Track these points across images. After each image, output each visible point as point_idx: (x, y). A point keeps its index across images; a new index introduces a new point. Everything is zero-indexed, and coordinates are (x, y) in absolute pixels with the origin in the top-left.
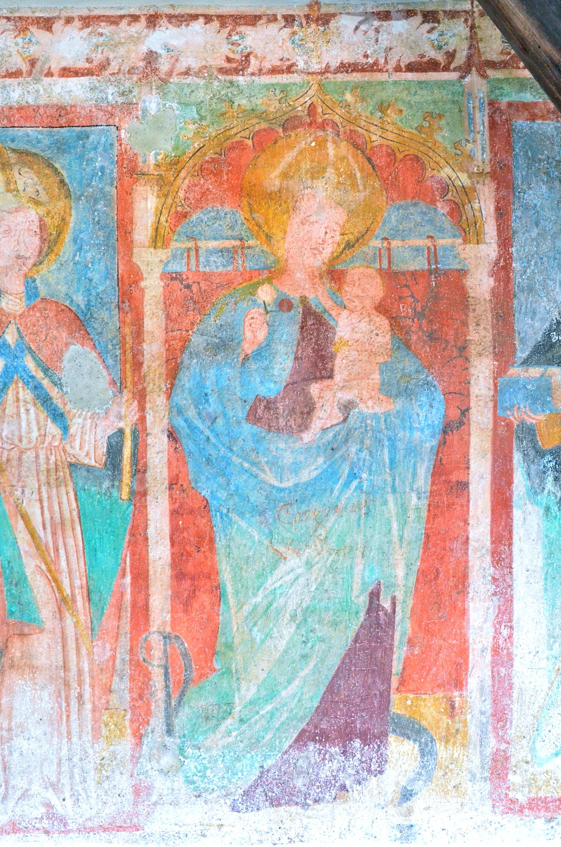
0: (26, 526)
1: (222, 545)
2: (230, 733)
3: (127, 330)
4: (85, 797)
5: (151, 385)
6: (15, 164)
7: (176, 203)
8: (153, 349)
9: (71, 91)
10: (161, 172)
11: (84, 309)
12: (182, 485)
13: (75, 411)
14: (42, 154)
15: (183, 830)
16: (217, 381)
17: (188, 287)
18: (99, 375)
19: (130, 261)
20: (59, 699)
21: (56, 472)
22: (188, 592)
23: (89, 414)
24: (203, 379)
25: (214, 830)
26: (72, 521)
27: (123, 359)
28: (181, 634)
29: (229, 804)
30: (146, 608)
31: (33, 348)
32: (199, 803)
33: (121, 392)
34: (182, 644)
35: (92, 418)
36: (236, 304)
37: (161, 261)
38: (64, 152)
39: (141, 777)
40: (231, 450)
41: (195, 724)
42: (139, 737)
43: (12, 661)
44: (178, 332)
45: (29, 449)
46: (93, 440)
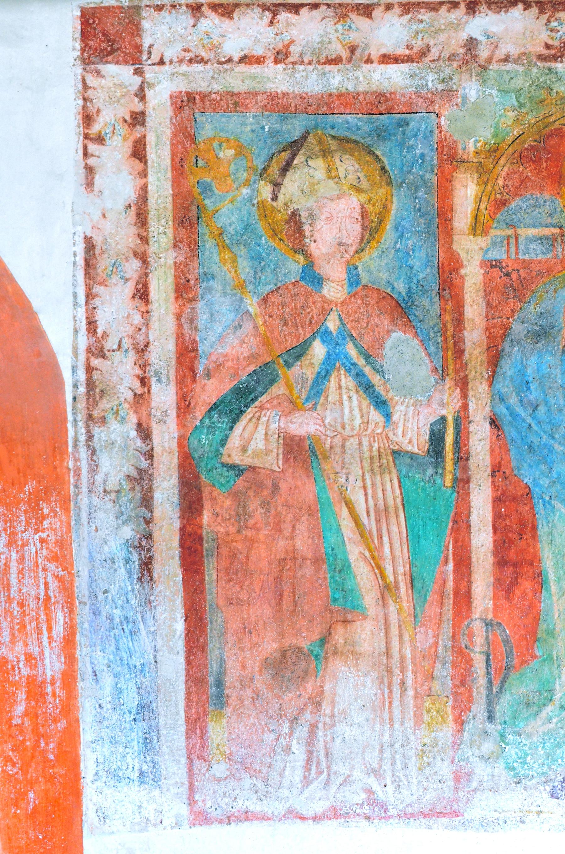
0: (350, 513)
1: (544, 533)
2: (551, 719)
3: (448, 318)
4: (406, 783)
5: (473, 372)
6: (336, 151)
7: (495, 190)
8: (474, 337)
9: (390, 78)
10: (481, 160)
11: (405, 296)
12: (504, 473)
13: (397, 398)
14: (363, 141)
15: (502, 816)
16: (538, 369)
17: (508, 274)
18: (422, 362)
19: (450, 248)
20: (382, 686)
21: (380, 459)
22: (510, 579)
23: (412, 401)
24: (525, 367)
25: (532, 817)
26: (396, 508)
27: (445, 346)
28: (503, 621)
29: (548, 790)
30: (468, 595)
31: (355, 335)
32: (519, 789)
33: (443, 379)
34: (504, 631)
35: (414, 405)
36: (556, 292)
37: (481, 249)
38: (384, 139)
39: (462, 763)
40: (553, 438)
41: (516, 711)
42: (460, 723)
43: (336, 648)
44: (499, 320)
45: (352, 436)
46: (416, 428)
